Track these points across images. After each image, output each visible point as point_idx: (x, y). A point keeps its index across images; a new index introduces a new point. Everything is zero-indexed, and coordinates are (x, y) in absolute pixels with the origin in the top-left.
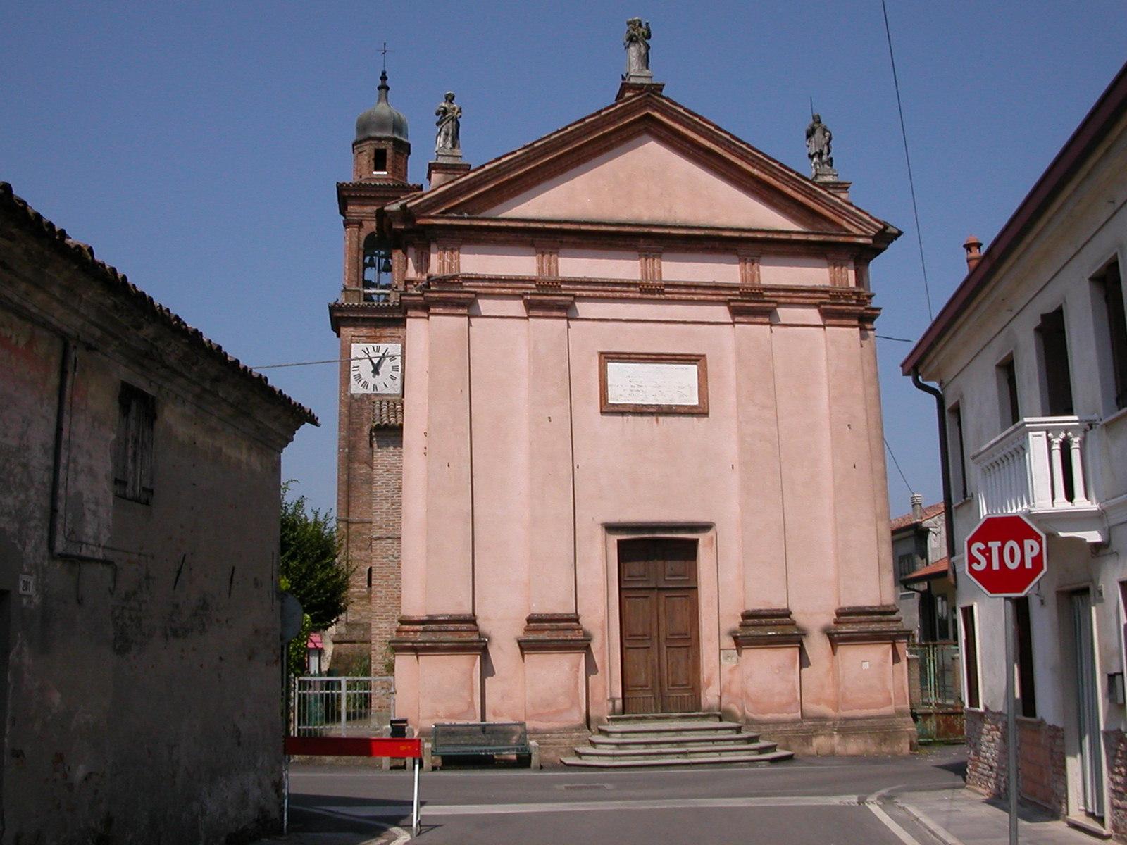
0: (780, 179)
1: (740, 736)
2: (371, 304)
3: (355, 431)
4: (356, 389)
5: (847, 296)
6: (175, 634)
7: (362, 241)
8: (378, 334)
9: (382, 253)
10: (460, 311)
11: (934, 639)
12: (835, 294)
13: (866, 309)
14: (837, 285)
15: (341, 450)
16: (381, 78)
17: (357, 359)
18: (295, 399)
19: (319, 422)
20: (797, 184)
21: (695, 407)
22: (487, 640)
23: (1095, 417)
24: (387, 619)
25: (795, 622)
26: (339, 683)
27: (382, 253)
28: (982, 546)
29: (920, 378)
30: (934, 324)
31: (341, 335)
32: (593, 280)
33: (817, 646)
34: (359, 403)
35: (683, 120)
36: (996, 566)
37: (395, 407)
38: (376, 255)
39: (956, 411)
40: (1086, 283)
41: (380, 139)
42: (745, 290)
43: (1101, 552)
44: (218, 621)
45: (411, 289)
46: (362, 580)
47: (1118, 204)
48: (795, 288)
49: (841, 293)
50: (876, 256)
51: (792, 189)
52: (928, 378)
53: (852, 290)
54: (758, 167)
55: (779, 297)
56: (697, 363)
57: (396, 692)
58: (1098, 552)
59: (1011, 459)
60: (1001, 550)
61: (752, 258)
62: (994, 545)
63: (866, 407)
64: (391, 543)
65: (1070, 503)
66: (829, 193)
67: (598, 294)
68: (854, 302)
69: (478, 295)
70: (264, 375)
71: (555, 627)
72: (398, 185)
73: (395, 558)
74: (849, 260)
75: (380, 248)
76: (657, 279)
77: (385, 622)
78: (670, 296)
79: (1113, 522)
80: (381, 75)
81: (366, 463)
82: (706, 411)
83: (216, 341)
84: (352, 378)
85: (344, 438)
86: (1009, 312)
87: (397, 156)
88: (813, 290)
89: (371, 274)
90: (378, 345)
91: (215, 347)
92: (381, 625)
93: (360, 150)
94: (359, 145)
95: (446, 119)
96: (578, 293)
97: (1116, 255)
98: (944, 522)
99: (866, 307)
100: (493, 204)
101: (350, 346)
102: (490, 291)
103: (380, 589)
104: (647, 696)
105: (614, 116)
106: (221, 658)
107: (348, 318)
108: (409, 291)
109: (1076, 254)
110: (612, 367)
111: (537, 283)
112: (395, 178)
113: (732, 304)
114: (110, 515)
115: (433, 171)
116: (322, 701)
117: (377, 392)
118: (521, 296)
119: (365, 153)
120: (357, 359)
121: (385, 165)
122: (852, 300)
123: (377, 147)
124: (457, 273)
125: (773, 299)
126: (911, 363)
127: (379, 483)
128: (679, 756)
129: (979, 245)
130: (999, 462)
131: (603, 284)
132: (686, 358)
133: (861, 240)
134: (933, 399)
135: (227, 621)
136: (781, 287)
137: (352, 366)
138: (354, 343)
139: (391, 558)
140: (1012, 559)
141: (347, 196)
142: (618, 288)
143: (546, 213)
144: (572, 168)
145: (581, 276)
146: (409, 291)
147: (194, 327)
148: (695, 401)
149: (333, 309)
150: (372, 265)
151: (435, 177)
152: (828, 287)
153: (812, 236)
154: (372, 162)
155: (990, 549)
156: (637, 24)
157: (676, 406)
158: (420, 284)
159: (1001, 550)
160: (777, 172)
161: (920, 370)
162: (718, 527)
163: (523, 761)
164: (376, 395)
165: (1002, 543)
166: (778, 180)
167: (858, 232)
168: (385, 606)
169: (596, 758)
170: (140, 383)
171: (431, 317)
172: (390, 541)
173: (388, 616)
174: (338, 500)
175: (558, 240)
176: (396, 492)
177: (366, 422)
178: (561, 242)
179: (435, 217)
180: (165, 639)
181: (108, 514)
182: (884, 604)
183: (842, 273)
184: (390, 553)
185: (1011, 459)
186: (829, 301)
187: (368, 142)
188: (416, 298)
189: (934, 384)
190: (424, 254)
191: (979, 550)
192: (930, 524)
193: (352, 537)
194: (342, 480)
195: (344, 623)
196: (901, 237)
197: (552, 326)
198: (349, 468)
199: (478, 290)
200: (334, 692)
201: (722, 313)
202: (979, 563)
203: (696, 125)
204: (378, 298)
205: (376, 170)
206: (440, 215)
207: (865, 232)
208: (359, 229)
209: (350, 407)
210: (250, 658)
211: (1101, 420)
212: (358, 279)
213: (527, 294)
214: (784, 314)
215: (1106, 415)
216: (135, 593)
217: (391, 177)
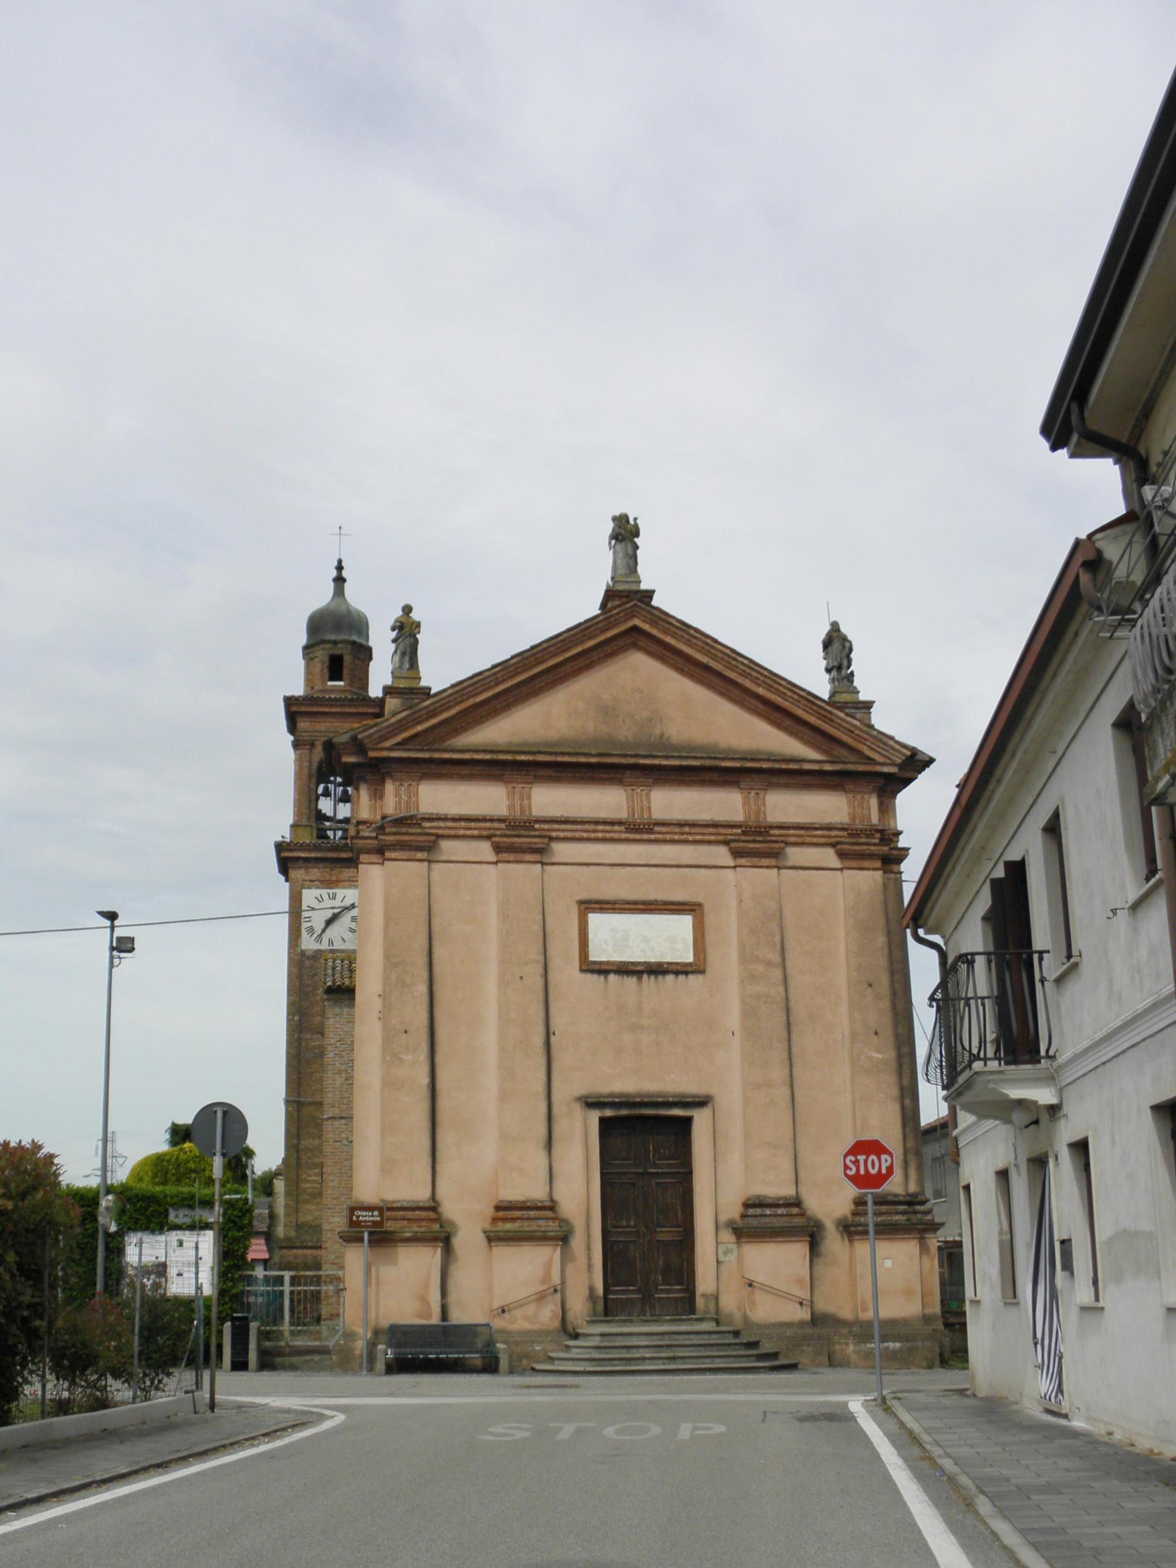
0: (790, 700)
1: (737, 1341)
2: (325, 841)
4: (308, 944)
5: (868, 835)
7: (315, 765)
8: (334, 878)
10: (419, 855)
12: (854, 832)
13: (891, 849)
14: (857, 822)
18: (582, 620)
20: (809, 705)
21: (690, 964)
24: (341, 1212)
26: (283, 1277)
27: (339, 780)
32: (571, 819)
33: (833, 1242)
34: (312, 961)
35: (676, 633)
36: (862, 1172)
37: (350, 966)
38: (331, 782)
41: (335, 643)
42: (748, 829)
45: (363, 831)
46: (315, 1174)
48: (808, 826)
49: (861, 831)
50: (905, 787)
51: (804, 710)
53: (875, 828)
54: (763, 685)
55: (788, 835)
56: (692, 913)
57: (346, 1289)
61: (757, 791)
64: (345, 1124)
66: (847, 714)
67: (577, 835)
68: (877, 841)
69: (438, 836)
71: (526, 1216)
72: (357, 698)
74: (871, 793)
76: (645, 817)
77: (338, 1217)
78: (660, 836)
82: (701, 968)
84: (304, 933)
87: (357, 662)
88: (829, 828)
90: (334, 891)
92: (333, 1220)
95: (404, 634)
96: (554, 834)
100: (457, 732)
101: (301, 893)
102: (452, 832)
103: (332, 1178)
105: (596, 630)
107: (298, 859)
108: (362, 834)
110: (594, 919)
111: (507, 823)
112: (354, 690)
113: (733, 845)
115: (388, 696)
117: (334, 948)
118: (488, 837)
122: (874, 838)
124: (416, 813)
125: (781, 839)
127: (331, 1055)
128: (664, 1361)
131: (583, 822)
132: (676, 907)
133: (886, 769)
134: (934, 954)
136: (791, 825)
138: (305, 888)
139: (345, 1142)
140: (873, 1167)
141: (295, 710)
142: (600, 827)
144: (548, 689)
145: (558, 814)
146: (362, 834)
148: (689, 958)
149: (280, 847)
150: (326, 793)
152: (847, 824)
153: (828, 764)
154: (326, 671)
156: (624, 521)
158: (374, 825)
160: (785, 691)
164: (332, 951)
166: (787, 700)
167: (880, 759)
168: (337, 1198)
169: (571, 1363)
171: (386, 862)
172: (343, 1121)
173: (342, 1209)
175: (531, 773)
178: (535, 776)
179: (390, 749)
183: (863, 807)
184: (343, 1135)
186: (848, 840)
187: (321, 647)
188: (369, 841)
189: (936, 939)
190: (378, 791)
195: (295, 1224)
196: (934, 764)
197: (524, 873)
199: (440, 832)
200: (276, 1288)
201: (722, 854)
202: (851, 1169)
203: (691, 638)
204: (335, 835)
205: (332, 679)
206: (396, 747)
207: (889, 758)
208: (310, 750)
212: (310, 813)
213: (495, 836)
214: (795, 855)
217: (349, 688)
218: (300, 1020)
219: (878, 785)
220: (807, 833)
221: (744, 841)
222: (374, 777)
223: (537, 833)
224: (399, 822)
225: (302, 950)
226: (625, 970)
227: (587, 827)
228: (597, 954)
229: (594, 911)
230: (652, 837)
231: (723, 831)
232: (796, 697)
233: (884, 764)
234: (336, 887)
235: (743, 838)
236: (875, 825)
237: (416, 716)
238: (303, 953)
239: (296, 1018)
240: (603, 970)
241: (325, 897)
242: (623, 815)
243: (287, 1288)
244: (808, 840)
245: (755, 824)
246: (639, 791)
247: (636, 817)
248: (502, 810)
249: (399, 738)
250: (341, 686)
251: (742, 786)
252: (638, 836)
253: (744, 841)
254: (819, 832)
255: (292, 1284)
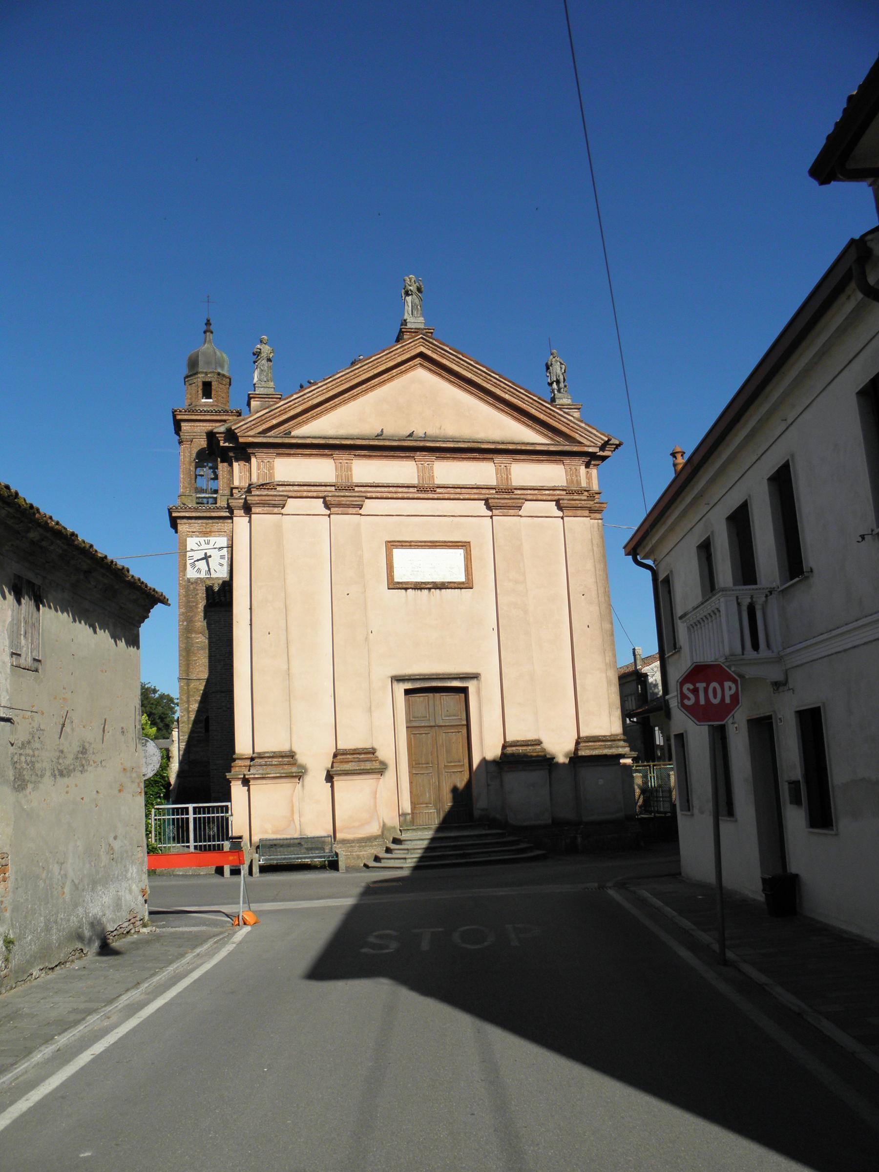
3: (191, 607)
6: (62, 774)
8: (208, 530)
9: (210, 465)
11: (13, 734)
15: (181, 623)
16: (206, 324)
17: (192, 550)
19: (169, 602)
21: (463, 583)
22: (303, 771)
23: (774, 585)
25: (545, 749)
26: (187, 809)
28: (691, 687)
29: (638, 557)
30: (648, 515)
31: (178, 532)
36: (702, 701)
39: (667, 581)
40: (765, 483)
43: (781, 689)
44: (94, 762)
47: (789, 422)
49: (575, 491)
52: (644, 558)
53: (584, 489)
58: (778, 689)
59: (713, 616)
60: (706, 690)
61: (505, 465)
62: (701, 686)
63: (597, 580)
65: (756, 652)
68: (585, 498)
70: (126, 566)
73: (228, 708)
75: (208, 461)
78: (441, 496)
79: (788, 666)
80: (206, 321)
81: (201, 633)
82: (471, 586)
83: (89, 540)
84: (188, 566)
85: (183, 614)
86: (706, 506)
89: (202, 483)
90: (209, 538)
91: (88, 546)
93: (190, 382)
94: (189, 379)
97: (788, 461)
98: (659, 669)
99: (595, 501)
100: (300, 425)
101: (186, 540)
104: (431, 811)
106: (97, 792)
109: (757, 460)
110: (396, 552)
114: (8, 681)
116: (173, 824)
119: (194, 384)
120: (192, 550)
121: (211, 394)
123: (204, 380)
125: (522, 497)
126: (632, 545)
129: (683, 454)
130: (701, 621)
132: (453, 544)
133: (591, 450)
134: (648, 573)
135: (101, 762)
137: (188, 556)
138: (189, 537)
140: (715, 696)
143: (331, 432)
147: (71, 531)
148: (462, 578)
151: (254, 403)
153: (552, 446)
155: (698, 688)
157: (448, 582)
159: (706, 690)
161: (638, 551)
162: (483, 678)
163: (333, 865)
165: (707, 685)
167: (588, 443)
170: (30, 575)
174: (179, 664)
176: (227, 656)
177: (200, 601)
180: (53, 779)
181: (6, 680)
182: (613, 733)
185: (713, 616)
189: (649, 562)
191: (688, 689)
192: (648, 670)
193: (191, 693)
194: (181, 647)
197: (343, 521)
198: (187, 638)
202: (689, 699)
206: (259, 435)
207: (594, 443)
209: (187, 588)
210: (120, 791)
211: (778, 588)
215: (782, 584)
216: (29, 742)
218: (187, 625)
219: (586, 460)
220: (538, 493)
221: (498, 499)
222: (417, 293)
223: (357, 494)
224: (261, 486)
225: (188, 578)
226: (418, 587)
227: (391, 489)
228: (399, 576)
229: (397, 547)
230: (436, 496)
231: (484, 491)
232: (531, 401)
233: (589, 446)
234: (210, 536)
235: (496, 496)
236: (585, 487)
237: (272, 413)
238: (189, 580)
239: (185, 623)
240: (404, 587)
241: (203, 543)
242: (415, 482)
243: (191, 816)
244: (540, 497)
245: (505, 487)
246: (426, 465)
247: (425, 482)
248: (331, 478)
249: (260, 429)
250: (211, 402)
251: (495, 462)
252: (425, 496)
253: (498, 499)
254: (547, 492)
255: (195, 813)
